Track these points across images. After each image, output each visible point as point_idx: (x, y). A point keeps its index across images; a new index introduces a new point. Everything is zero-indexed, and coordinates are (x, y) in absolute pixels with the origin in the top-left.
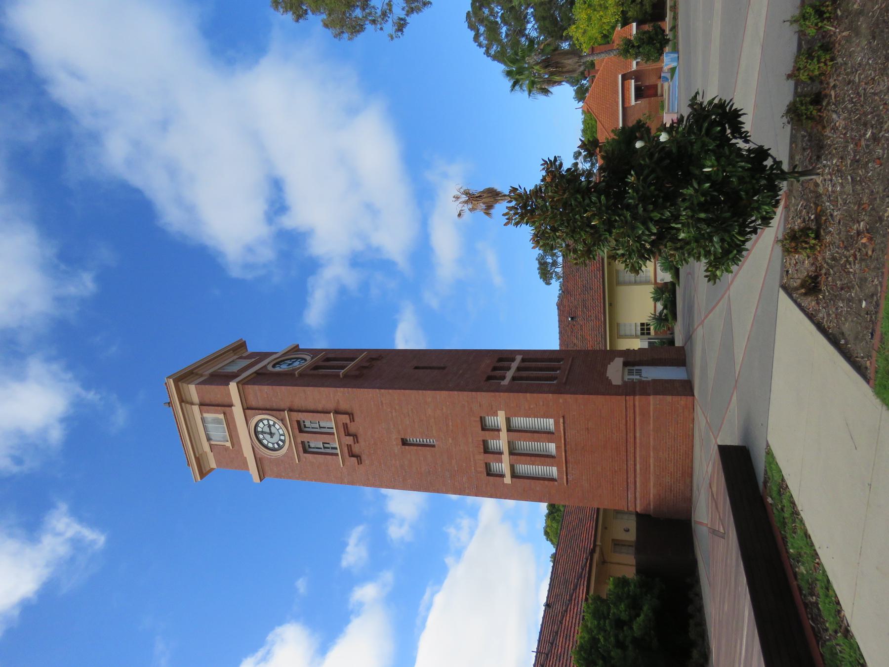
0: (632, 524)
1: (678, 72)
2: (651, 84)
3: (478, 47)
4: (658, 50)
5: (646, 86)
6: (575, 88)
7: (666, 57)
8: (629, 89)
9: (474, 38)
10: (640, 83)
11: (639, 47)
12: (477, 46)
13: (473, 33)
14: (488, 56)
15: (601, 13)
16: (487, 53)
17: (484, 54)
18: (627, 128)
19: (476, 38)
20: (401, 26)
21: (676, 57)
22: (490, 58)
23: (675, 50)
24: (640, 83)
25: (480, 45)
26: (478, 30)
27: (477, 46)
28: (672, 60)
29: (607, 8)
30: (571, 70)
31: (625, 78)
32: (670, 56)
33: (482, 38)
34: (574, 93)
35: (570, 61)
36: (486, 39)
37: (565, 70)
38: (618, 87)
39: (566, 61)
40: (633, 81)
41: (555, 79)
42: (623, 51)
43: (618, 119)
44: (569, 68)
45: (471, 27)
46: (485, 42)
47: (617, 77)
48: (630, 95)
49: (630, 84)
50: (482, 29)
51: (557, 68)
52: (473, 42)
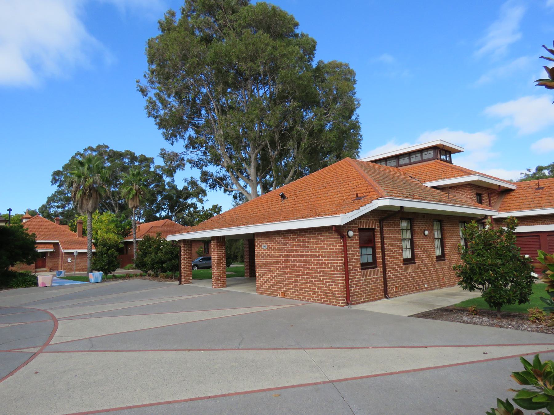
0: (364, 251)
1: (80, 284)
2: (46, 263)
3: (84, 149)
4: (102, 268)
5: (46, 260)
6: (37, 211)
7: (100, 274)
8: (46, 248)
9: (91, 147)
10: (49, 256)
11: (107, 253)
12: (86, 148)
13: (94, 147)
14: (76, 154)
15: (104, 229)
16: (78, 154)
17: (78, 152)
18: (36, 246)
19: (91, 149)
20: (143, 91)
21: (98, 280)
22: (74, 155)
23: (103, 280)
24: (49, 256)
25: (85, 150)
26: (95, 151)
27: (86, 148)
28: (97, 278)
29: (107, 233)
30: (83, 206)
31: (56, 245)
32: (100, 276)
33: (90, 152)
34: (33, 209)
35: (90, 205)
36: (89, 155)
37: (84, 201)
38: (49, 240)
39: (91, 202)
40: (52, 250)
41: (79, 193)
42: (105, 243)
43: (541, 207)
44: (85, 205)
45: (99, 147)
46: (87, 154)
47: (57, 239)
48: (44, 248)
49: (49, 248)
50: (95, 154)
51: (88, 195)
52: (88, 146)
